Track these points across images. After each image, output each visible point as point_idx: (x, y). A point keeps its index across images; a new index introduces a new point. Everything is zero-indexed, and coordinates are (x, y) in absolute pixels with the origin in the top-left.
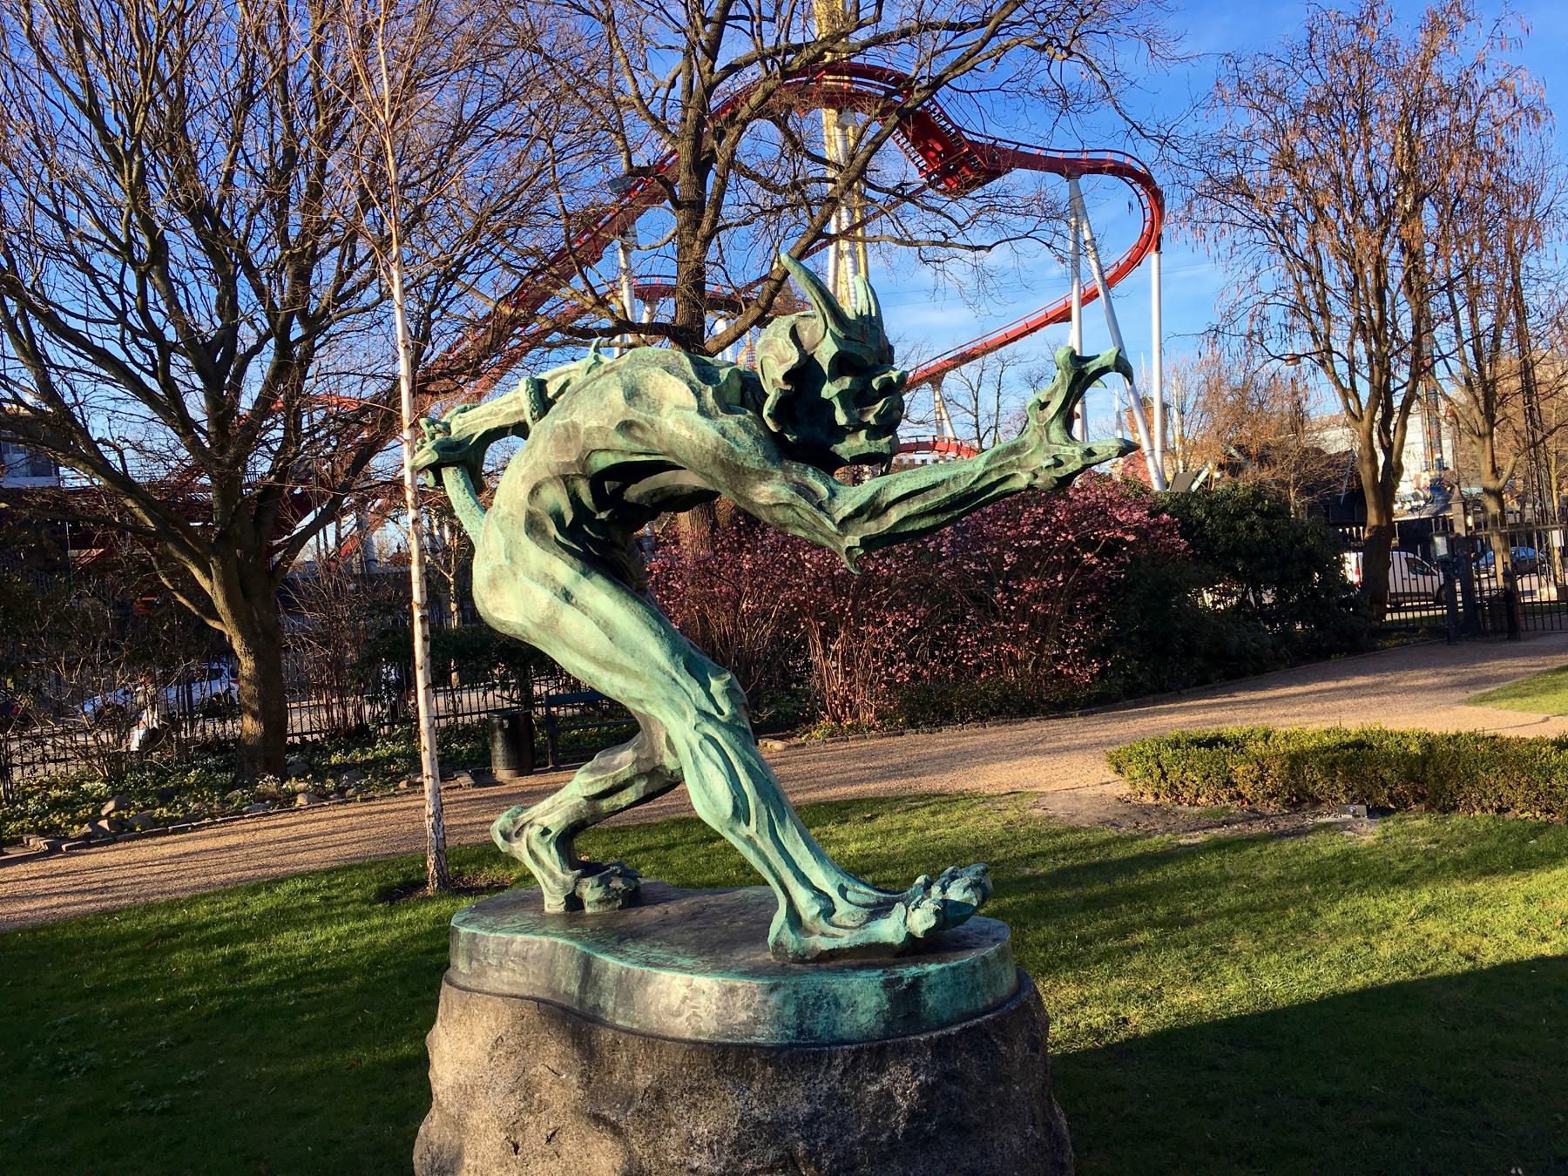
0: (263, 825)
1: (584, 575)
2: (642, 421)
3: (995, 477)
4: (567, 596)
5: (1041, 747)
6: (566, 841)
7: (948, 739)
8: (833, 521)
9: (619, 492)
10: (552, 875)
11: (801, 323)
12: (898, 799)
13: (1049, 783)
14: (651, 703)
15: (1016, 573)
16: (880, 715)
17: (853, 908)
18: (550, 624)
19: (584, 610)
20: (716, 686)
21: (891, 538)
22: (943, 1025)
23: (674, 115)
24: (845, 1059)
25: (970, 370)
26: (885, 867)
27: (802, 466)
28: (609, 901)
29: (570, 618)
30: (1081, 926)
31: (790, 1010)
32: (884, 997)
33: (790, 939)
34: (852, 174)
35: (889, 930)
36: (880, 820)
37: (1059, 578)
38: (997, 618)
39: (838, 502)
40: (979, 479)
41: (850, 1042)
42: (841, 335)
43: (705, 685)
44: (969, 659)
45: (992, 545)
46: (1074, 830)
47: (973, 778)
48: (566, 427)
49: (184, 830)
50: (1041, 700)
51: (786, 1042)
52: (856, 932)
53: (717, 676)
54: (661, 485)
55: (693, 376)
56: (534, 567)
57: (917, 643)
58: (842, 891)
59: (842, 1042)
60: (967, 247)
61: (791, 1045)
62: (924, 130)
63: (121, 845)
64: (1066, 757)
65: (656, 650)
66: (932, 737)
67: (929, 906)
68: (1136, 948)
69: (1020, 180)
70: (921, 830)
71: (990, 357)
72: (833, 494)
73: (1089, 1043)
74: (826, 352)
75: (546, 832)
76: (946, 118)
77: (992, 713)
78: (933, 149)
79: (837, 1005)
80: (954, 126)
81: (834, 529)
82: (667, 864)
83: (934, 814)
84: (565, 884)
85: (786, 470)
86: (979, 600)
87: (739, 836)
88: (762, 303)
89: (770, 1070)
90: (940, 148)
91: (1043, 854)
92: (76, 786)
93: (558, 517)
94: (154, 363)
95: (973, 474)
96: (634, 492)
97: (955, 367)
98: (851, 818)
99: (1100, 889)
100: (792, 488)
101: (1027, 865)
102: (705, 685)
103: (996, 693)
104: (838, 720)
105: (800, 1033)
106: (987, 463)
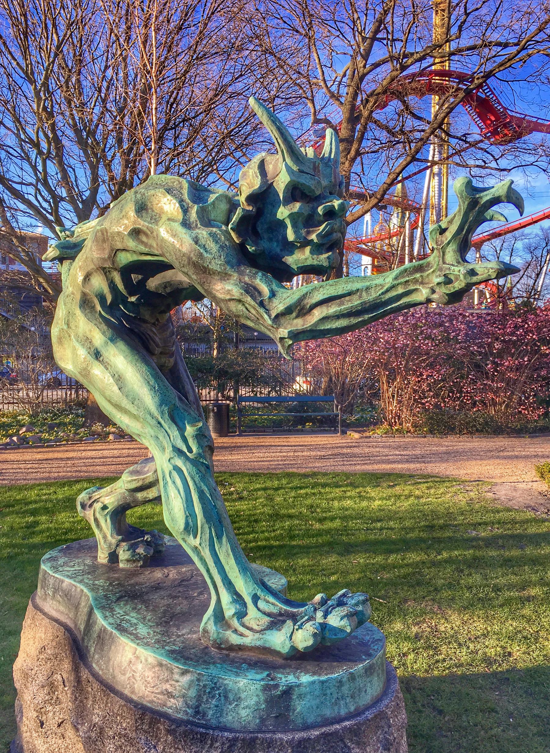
0: (89, 448)
1: (112, 340)
2: (145, 229)
3: (400, 290)
4: (97, 355)
5: (502, 454)
6: (118, 514)
7: (451, 442)
8: (270, 316)
9: (142, 283)
10: (105, 537)
11: (268, 158)
12: (411, 476)
13: (501, 477)
14: (145, 438)
15: (500, 354)
16: (415, 426)
17: (259, 615)
18: (86, 372)
19: (106, 366)
20: (190, 430)
21: (313, 334)
22: (307, 727)
23: (344, 91)
24: (223, 744)
25: (497, 242)
26: (390, 519)
27: (254, 270)
28: (134, 561)
29: (97, 371)
30: (497, 578)
31: (192, 693)
32: (262, 698)
33: (212, 628)
34: (436, 125)
35: (279, 640)
36: (397, 488)
37: (526, 359)
38: (487, 378)
39: (276, 301)
40: (387, 291)
41: (231, 730)
42: (295, 168)
43: (182, 430)
44: (467, 400)
45: (488, 338)
46: (509, 510)
47: (458, 468)
48: (102, 231)
49: (52, 446)
50: (507, 426)
51: (185, 718)
52: (257, 635)
53: (192, 424)
54: (168, 279)
55: (186, 197)
56: (81, 331)
57: (441, 388)
58: (255, 599)
59: (225, 729)
60: (496, 169)
61: (188, 722)
62: (485, 108)
63: (20, 451)
64: (515, 462)
65: (149, 400)
66: (441, 440)
67: (310, 628)
68: (529, 599)
69: (536, 137)
70: (418, 497)
71: (509, 235)
72: (273, 294)
73: (482, 668)
74: (282, 182)
75: (105, 508)
76: (499, 103)
77: (477, 430)
78: (490, 119)
79: (226, 697)
80: (503, 107)
81: (270, 322)
82: (272, 500)
83: (428, 488)
84: (110, 545)
85: (241, 273)
86: (478, 367)
87: (189, 545)
88: (379, 196)
89: (170, 738)
90: (493, 119)
91: (486, 524)
92: (15, 417)
93: (102, 298)
94: (52, 208)
95: (382, 286)
96: (153, 283)
97: (489, 240)
98: (382, 484)
99: (515, 553)
100: (242, 288)
101: (474, 529)
102: (182, 430)
103: (481, 420)
104: (391, 425)
105: (197, 713)
106: (396, 278)
